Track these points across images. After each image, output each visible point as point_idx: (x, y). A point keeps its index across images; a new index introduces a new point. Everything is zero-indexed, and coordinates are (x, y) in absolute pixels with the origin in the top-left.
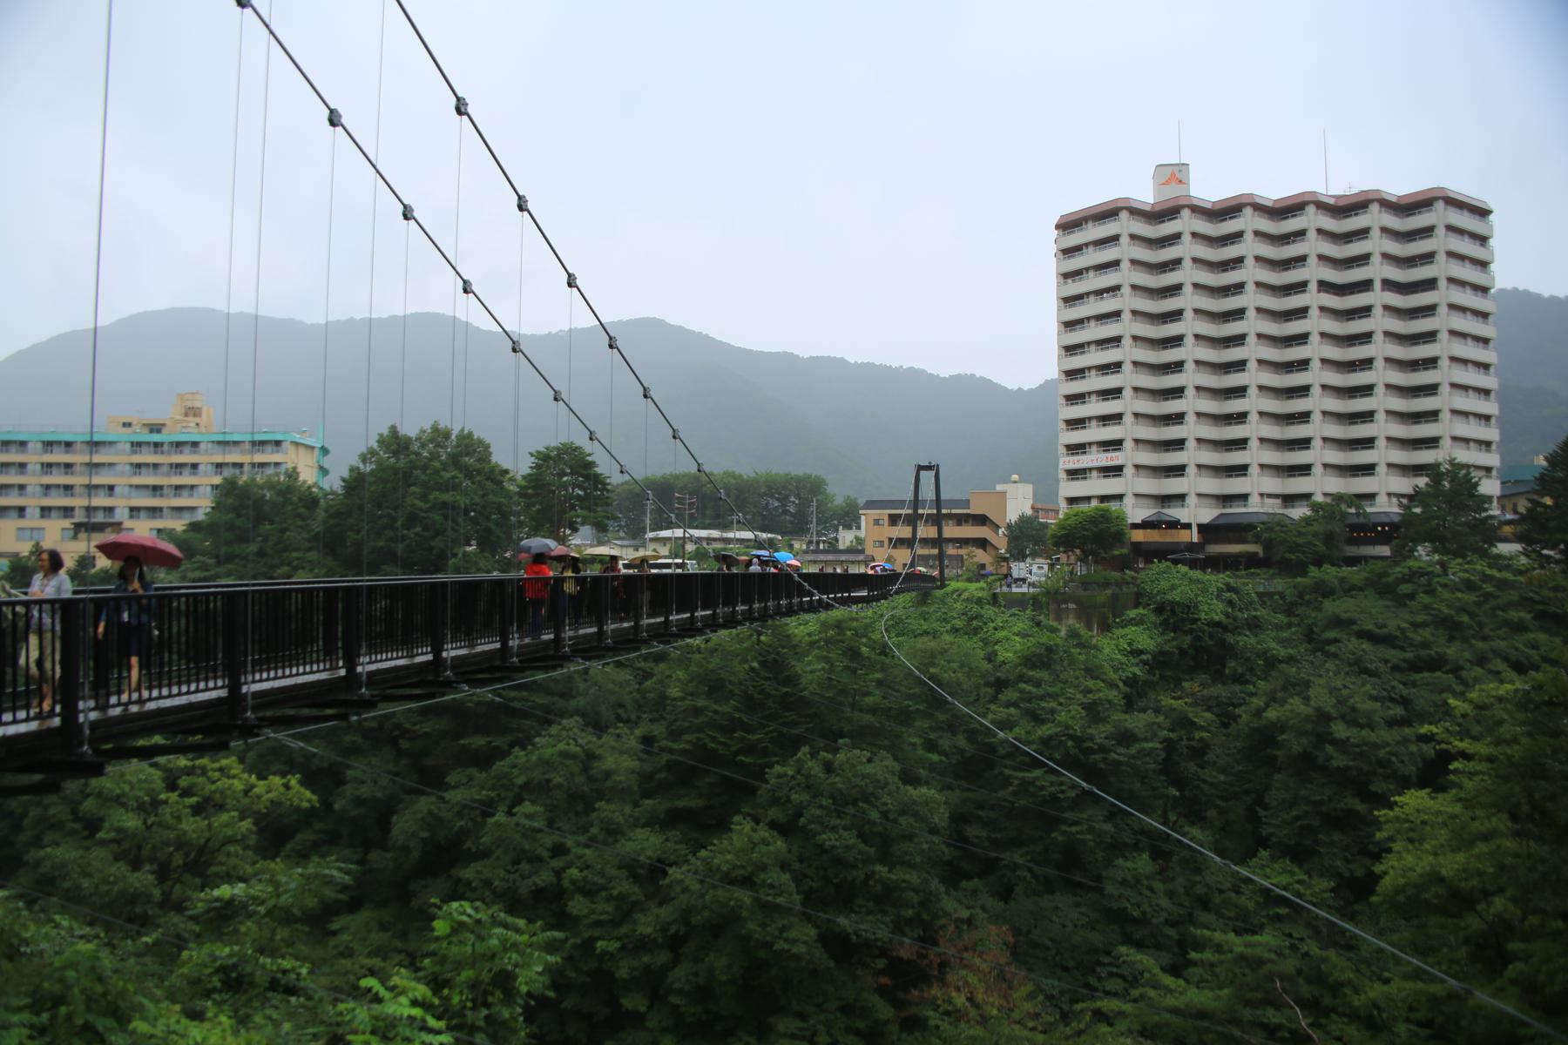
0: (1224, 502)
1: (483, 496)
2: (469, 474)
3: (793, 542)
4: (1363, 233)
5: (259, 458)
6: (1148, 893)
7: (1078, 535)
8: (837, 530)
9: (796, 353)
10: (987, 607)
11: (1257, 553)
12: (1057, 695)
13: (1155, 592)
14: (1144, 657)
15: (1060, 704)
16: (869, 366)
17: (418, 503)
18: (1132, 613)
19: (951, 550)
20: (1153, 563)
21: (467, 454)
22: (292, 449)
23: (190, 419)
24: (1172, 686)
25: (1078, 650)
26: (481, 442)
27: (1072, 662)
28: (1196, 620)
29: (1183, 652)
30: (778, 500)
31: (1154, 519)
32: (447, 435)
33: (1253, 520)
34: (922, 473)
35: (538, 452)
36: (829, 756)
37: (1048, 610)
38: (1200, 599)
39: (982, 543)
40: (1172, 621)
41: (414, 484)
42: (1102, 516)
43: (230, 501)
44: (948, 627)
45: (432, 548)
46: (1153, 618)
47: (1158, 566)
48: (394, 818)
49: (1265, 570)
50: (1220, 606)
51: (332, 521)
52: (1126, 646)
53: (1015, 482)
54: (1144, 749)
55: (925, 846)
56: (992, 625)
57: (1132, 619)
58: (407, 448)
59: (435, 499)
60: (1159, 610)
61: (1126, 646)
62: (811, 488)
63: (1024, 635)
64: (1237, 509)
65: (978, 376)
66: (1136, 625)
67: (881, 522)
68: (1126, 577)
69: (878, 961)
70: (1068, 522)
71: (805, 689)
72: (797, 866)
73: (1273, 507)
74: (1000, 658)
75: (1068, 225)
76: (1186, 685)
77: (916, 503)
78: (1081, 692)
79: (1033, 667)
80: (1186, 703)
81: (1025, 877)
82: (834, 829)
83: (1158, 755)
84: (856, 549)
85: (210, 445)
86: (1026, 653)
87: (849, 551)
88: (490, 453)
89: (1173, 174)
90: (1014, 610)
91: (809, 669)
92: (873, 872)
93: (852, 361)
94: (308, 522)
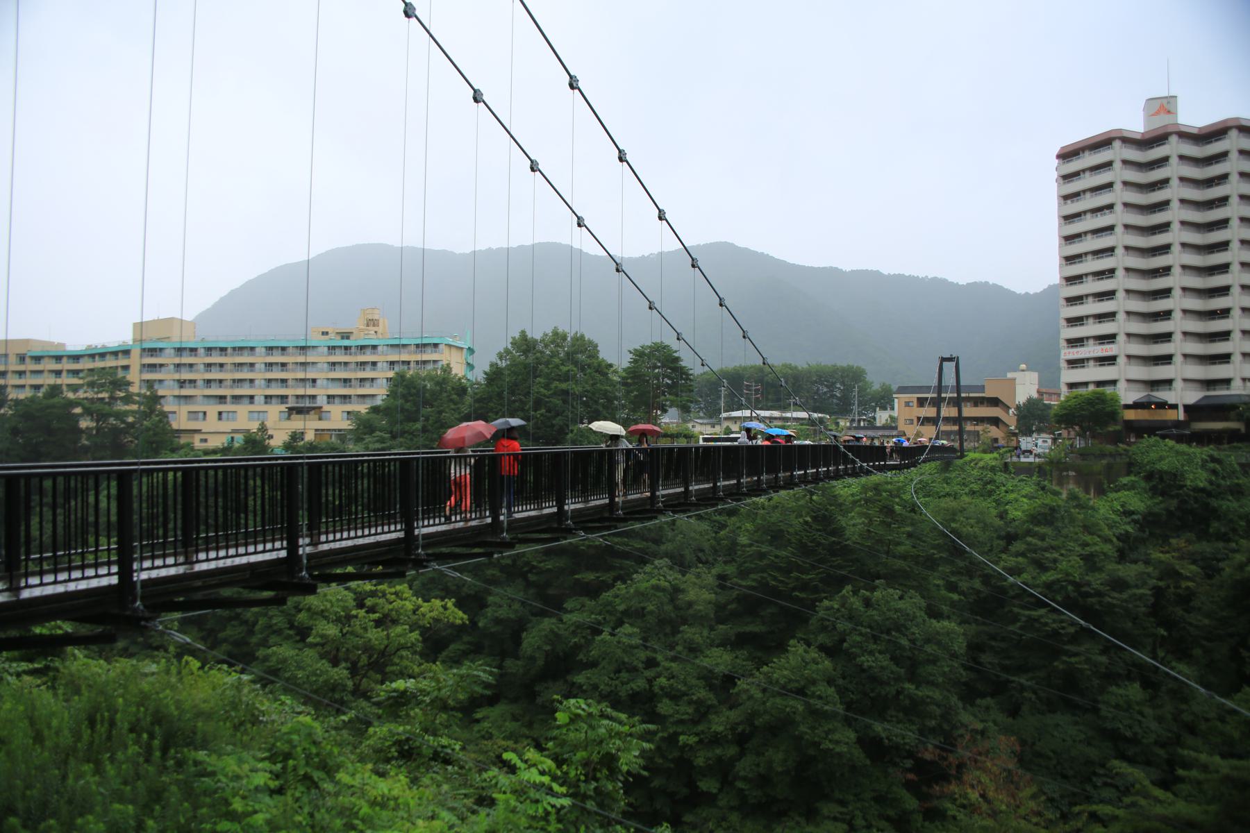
1: (593, 385)
4: (1163, 161)
8: (875, 411)
11: (1239, 430)
12: (1059, 547)
19: (969, 427)
20: (1143, 437)
22: (446, 351)
26: (590, 342)
28: (1182, 487)
29: (1170, 513)
31: (1144, 400)
32: (564, 338)
33: (1235, 401)
34: (945, 364)
35: (635, 350)
36: (868, 594)
37: (1051, 475)
39: (996, 421)
40: (1160, 487)
42: (1098, 398)
43: (400, 390)
44: (967, 490)
45: (553, 426)
46: (1143, 484)
47: (1148, 441)
51: (477, 405)
54: (1135, 595)
55: (946, 669)
59: (556, 387)
60: (1149, 477)
62: (853, 376)
64: (1221, 392)
66: (1128, 490)
69: (905, 761)
72: (840, 682)
74: (1010, 516)
75: (1067, 155)
77: (940, 388)
79: (1038, 523)
80: (1173, 557)
82: (871, 653)
84: (891, 426)
85: (385, 348)
89: (1162, 106)
90: (1022, 477)
91: (852, 522)
94: (459, 406)
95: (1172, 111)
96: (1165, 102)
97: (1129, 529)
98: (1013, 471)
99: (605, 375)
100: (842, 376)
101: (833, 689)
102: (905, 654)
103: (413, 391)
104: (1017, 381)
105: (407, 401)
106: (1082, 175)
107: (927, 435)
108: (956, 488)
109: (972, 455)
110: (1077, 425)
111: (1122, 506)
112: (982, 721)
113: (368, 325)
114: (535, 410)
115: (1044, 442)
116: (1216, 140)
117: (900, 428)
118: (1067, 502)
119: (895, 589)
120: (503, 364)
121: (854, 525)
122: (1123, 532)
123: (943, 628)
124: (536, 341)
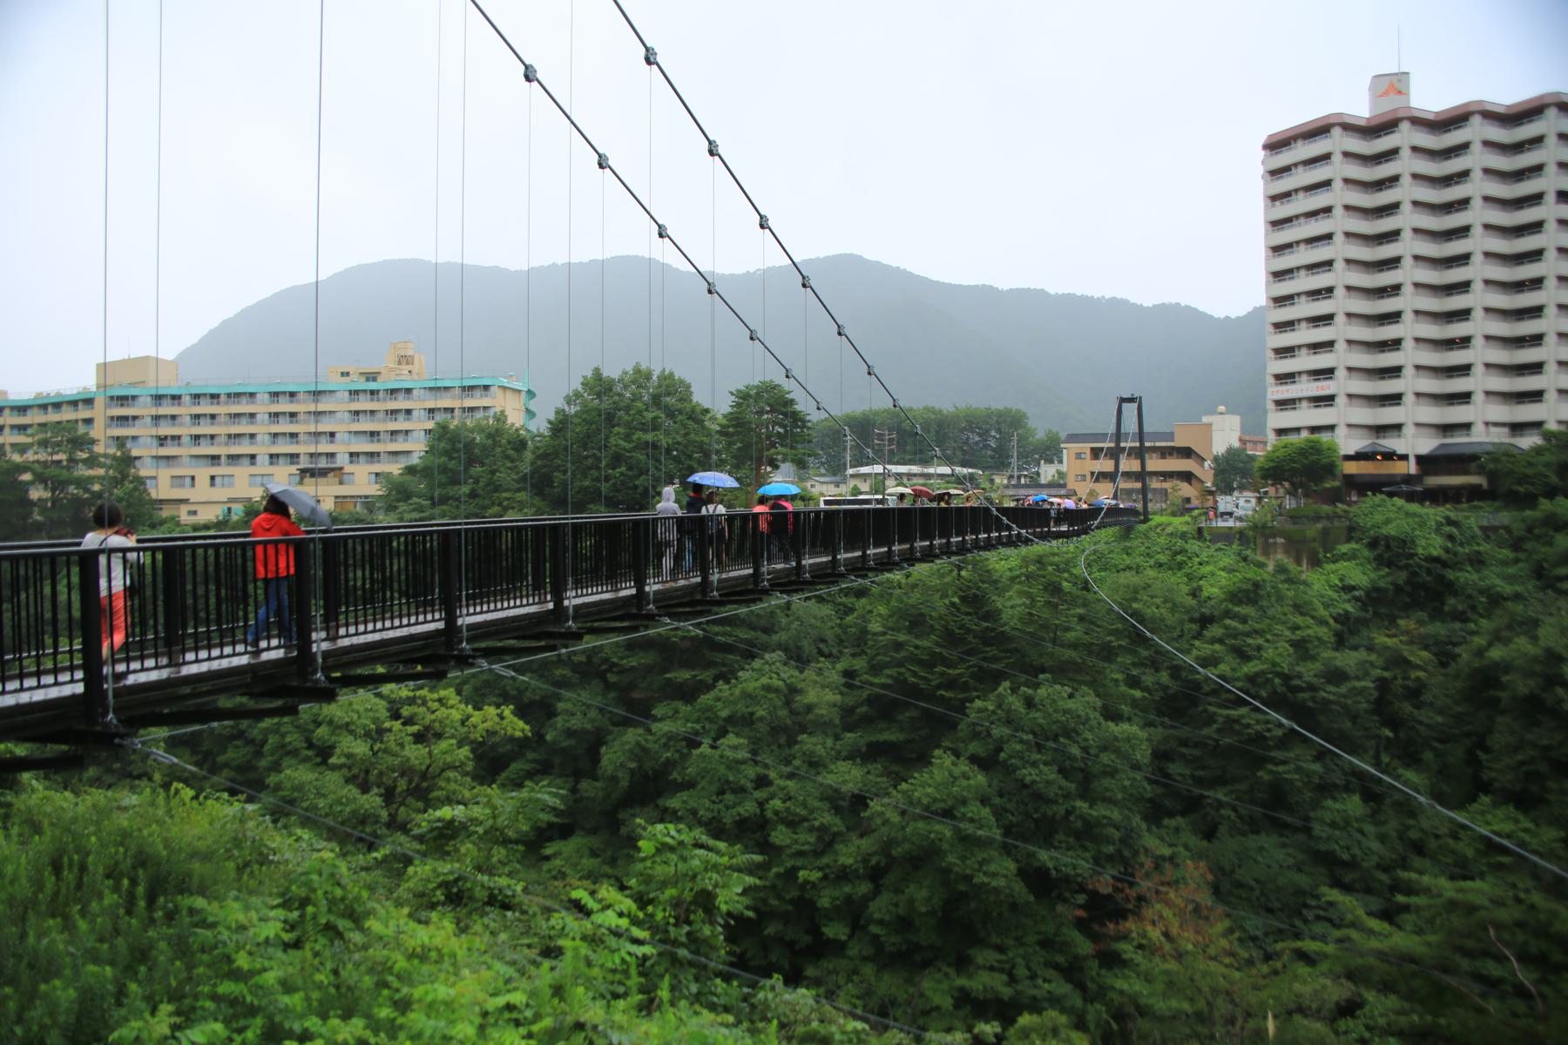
1: (686, 435)
2: (671, 414)
5: (469, 403)
8: (1039, 465)
10: (1191, 541)
11: (1479, 486)
12: (1264, 631)
14: (1357, 593)
15: (1268, 641)
16: (1070, 298)
18: (1344, 548)
19: (1155, 484)
20: (1366, 495)
21: (669, 394)
22: (499, 393)
28: (1412, 556)
33: (1476, 450)
34: (1125, 405)
35: (738, 391)
36: (1030, 691)
38: (1417, 533)
39: (1187, 477)
40: (1386, 555)
41: (618, 425)
42: (1312, 448)
43: (442, 445)
44: (1152, 562)
45: (636, 487)
48: (603, 749)
49: (1489, 502)
50: (1438, 541)
51: (539, 463)
52: (1337, 582)
54: (1355, 688)
55: (1127, 783)
56: (1197, 560)
59: (639, 439)
60: (1373, 544)
61: (1337, 582)
62: (1011, 422)
63: (1230, 571)
64: (1459, 439)
66: (1348, 560)
71: (1005, 624)
72: (997, 800)
73: (1500, 436)
74: (1205, 594)
75: (1276, 145)
76: (1402, 622)
77: (1118, 435)
79: (1240, 603)
82: (1034, 764)
84: (1057, 485)
87: (1050, 485)
88: (691, 393)
89: (1391, 85)
90: (1219, 545)
91: (1009, 604)
92: (1074, 807)
95: (1403, 90)
96: (1395, 79)
100: (998, 423)
101: (987, 810)
104: (1214, 428)
106: (1294, 170)
108: (1139, 560)
109: (1157, 519)
111: (1341, 580)
112: (1171, 845)
113: (400, 363)
117: (1070, 486)
121: (1012, 607)
123: (1123, 732)
124: (613, 380)
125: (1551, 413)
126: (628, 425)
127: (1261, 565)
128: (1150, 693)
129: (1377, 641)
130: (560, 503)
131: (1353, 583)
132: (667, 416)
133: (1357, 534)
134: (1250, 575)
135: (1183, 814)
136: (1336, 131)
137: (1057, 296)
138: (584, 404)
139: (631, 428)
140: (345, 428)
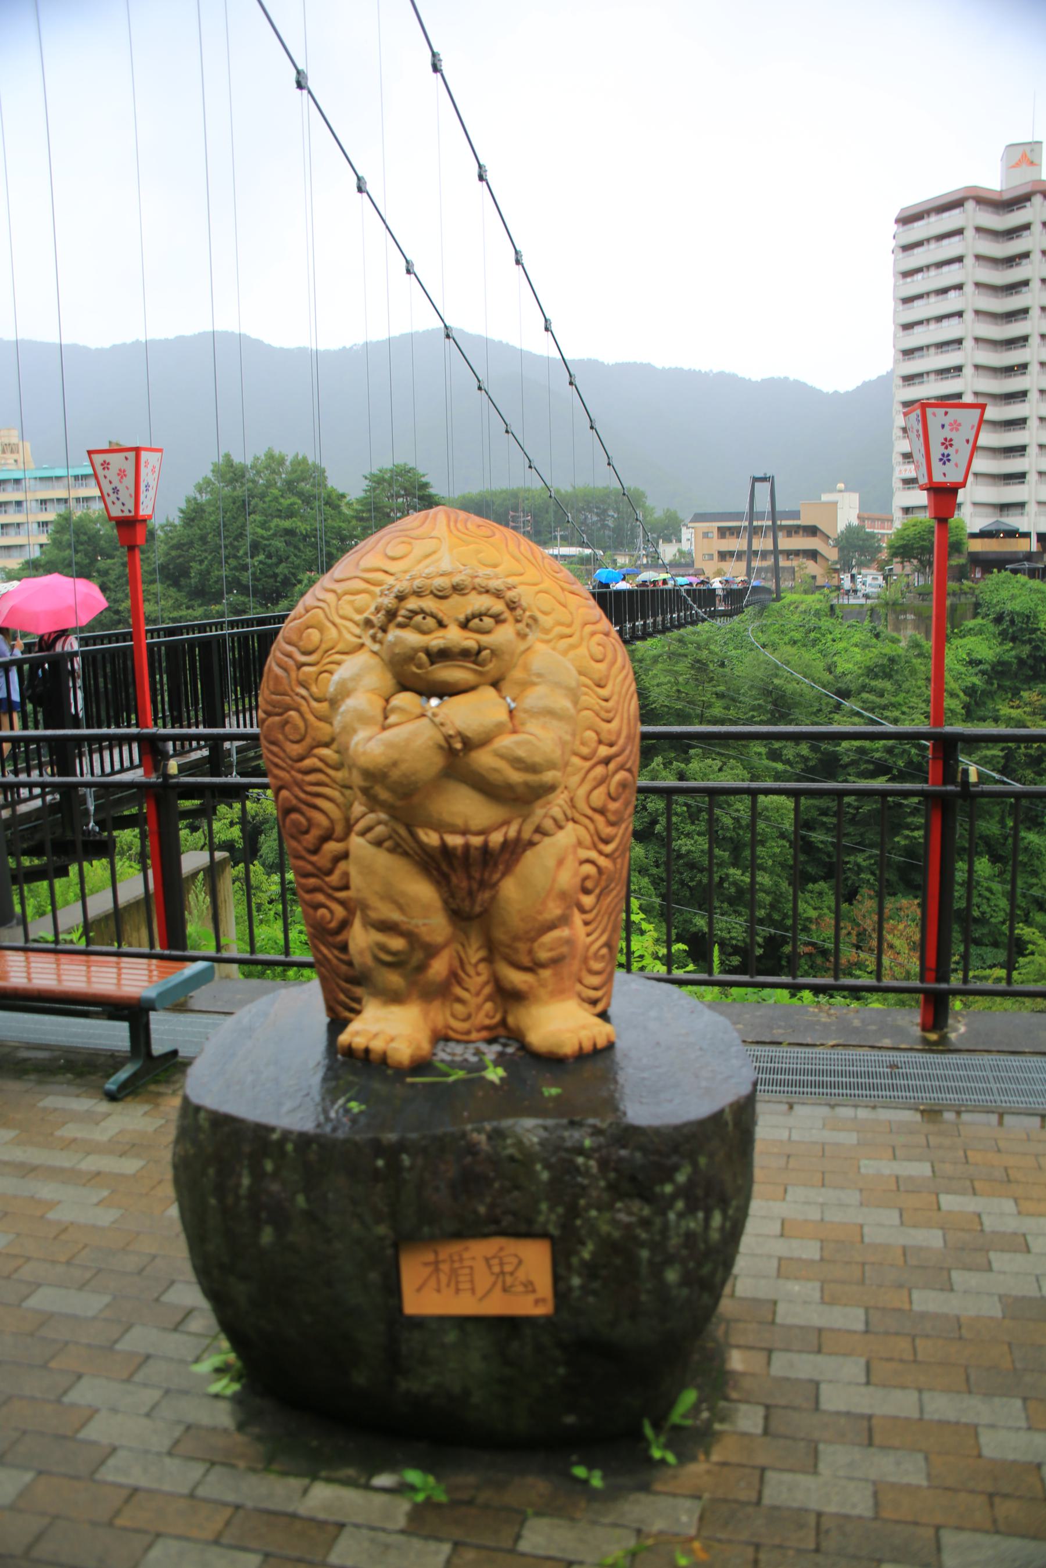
0: (1001, 511)
2: (307, 499)
3: (616, 557)
6: (987, 894)
7: (916, 546)
9: (600, 360)
10: (825, 618)
12: (900, 704)
13: (994, 601)
14: (981, 667)
15: (903, 713)
16: (678, 372)
17: (259, 531)
18: (970, 623)
19: (783, 563)
20: (992, 572)
21: (304, 479)
23: (8, 455)
24: (1010, 695)
25: (919, 661)
27: (913, 672)
28: (1035, 630)
29: (1021, 662)
30: (598, 515)
31: (993, 528)
32: (281, 462)
34: (757, 484)
35: (374, 475)
36: (683, 766)
37: (886, 620)
38: (1040, 608)
39: (813, 555)
40: (1011, 630)
41: (254, 512)
43: (66, 537)
44: (786, 639)
45: (275, 575)
47: (996, 576)
48: (262, 838)
51: (174, 553)
52: (964, 656)
53: (841, 491)
54: (986, 757)
55: (777, 850)
56: (830, 637)
57: (971, 629)
58: (243, 476)
59: (277, 526)
60: (999, 619)
61: (964, 656)
63: (866, 646)
65: (791, 379)
66: (975, 635)
67: (710, 535)
68: (963, 587)
69: (731, 958)
70: (907, 532)
71: (654, 702)
72: (654, 871)
74: (839, 670)
75: (907, 219)
76: (1023, 694)
77: (752, 515)
78: (924, 701)
79: (876, 677)
80: (1025, 712)
81: (868, 880)
82: (688, 835)
83: (998, 763)
84: (683, 563)
85: (32, 482)
86: (868, 664)
87: (674, 564)
88: (326, 478)
89: (1024, 155)
90: (852, 622)
91: (655, 682)
92: (727, 875)
93: (885, 373)
94: (149, 554)
95: (1035, 162)
96: (1028, 148)
97: (976, 680)
98: (840, 615)
99: (336, 507)
100: (616, 502)
101: (646, 879)
102: (728, 835)
103: (84, 538)
104: (839, 505)
105: (76, 552)
107: (736, 572)
108: (775, 638)
109: (789, 597)
110: (915, 558)
111: (968, 654)
112: (815, 909)
113: (4, 452)
114: (252, 557)
115: (874, 579)
116: (1018, 209)
117: (697, 565)
118: (907, 650)
119: (714, 759)
120: (204, 498)
121: (658, 685)
122: (969, 684)
123: (772, 803)
124: (246, 467)
125: (1033, 522)
126: (264, 512)
127: (895, 641)
128: (791, 765)
129: (1002, 712)
130: (203, 594)
131: (979, 657)
132: (303, 501)
133: (982, 610)
134: (886, 650)
135: (825, 879)
136: (970, 205)
137: (664, 371)
138: (212, 492)
139: (269, 516)
140: (32, 518)
